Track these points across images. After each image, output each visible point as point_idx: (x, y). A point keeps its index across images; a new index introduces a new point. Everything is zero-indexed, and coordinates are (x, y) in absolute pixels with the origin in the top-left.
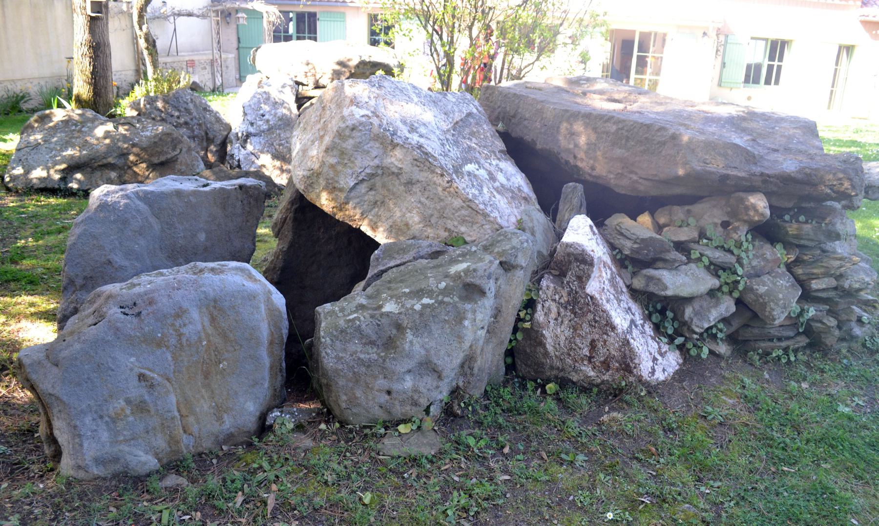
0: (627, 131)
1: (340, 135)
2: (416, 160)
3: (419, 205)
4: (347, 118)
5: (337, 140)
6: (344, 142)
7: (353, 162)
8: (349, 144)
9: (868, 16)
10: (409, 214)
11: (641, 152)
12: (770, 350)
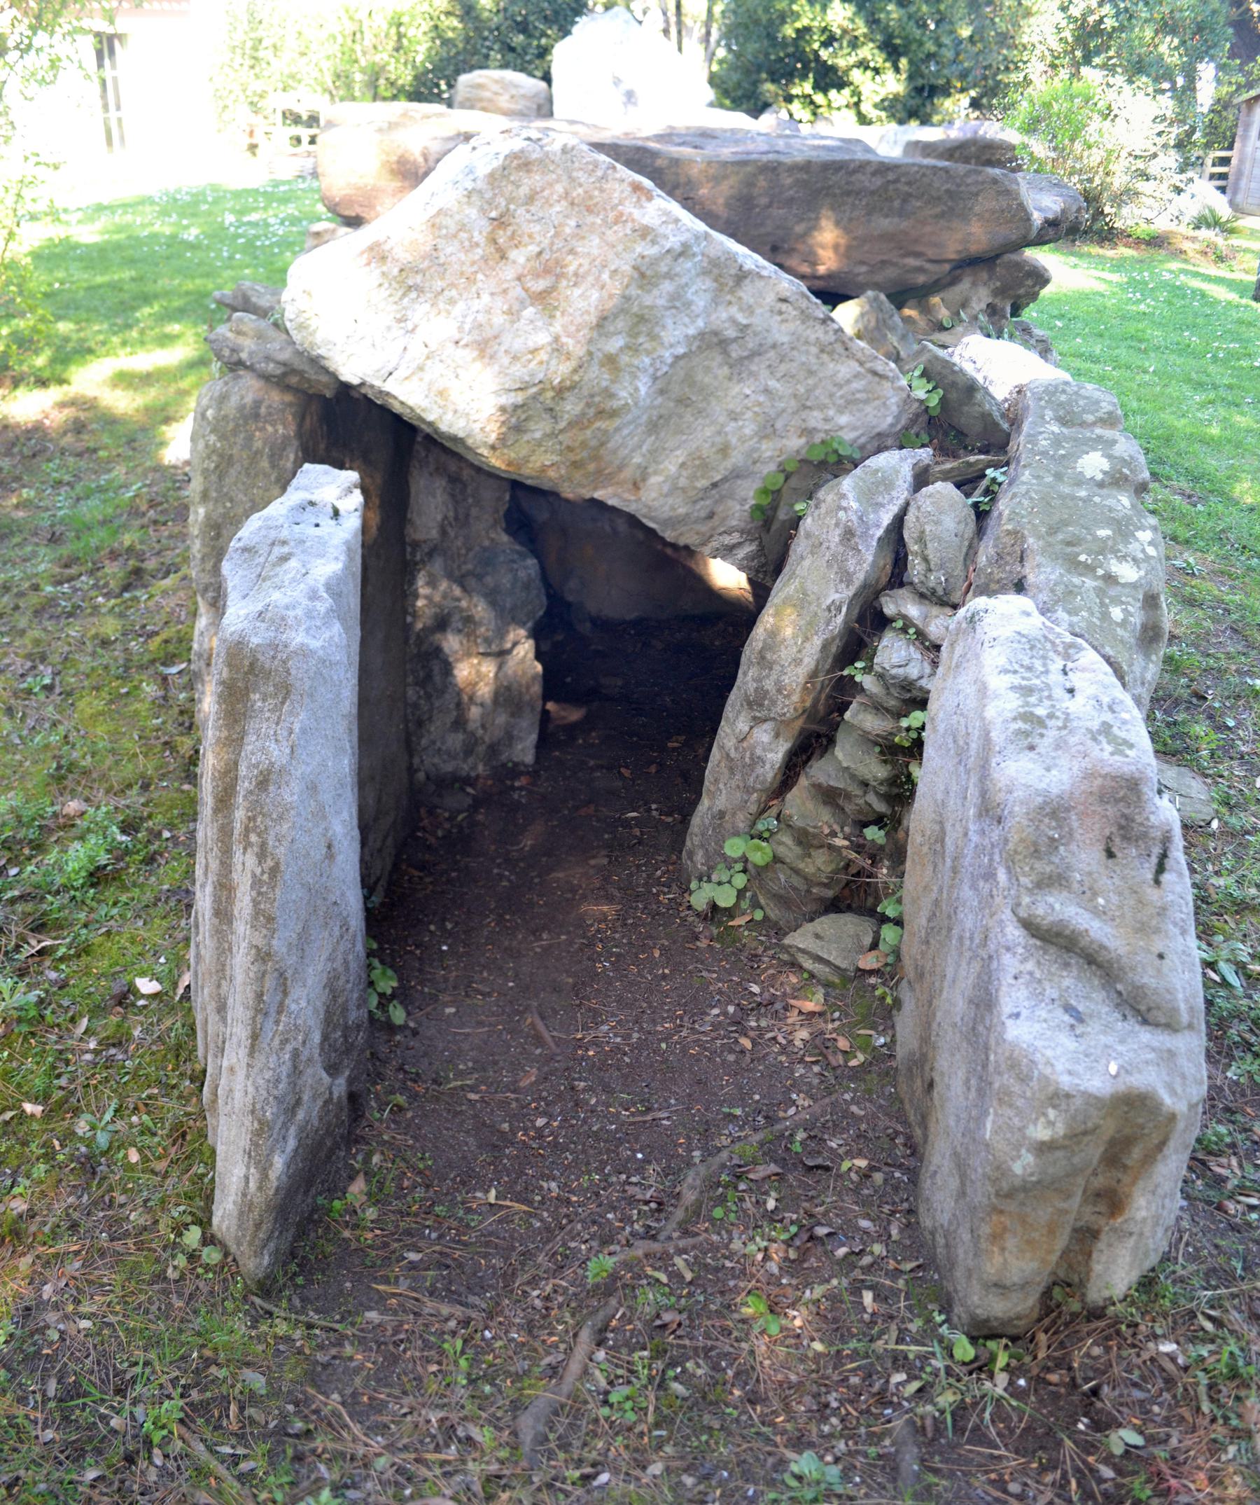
0: (909, 183)
1: (643, 275)
2: (784, 300)
3: (762, 399)
4: (662, 230)
5: (634, 291)
6: (649, 291)
7: (653, 337)
8: (658, 297)
9: (118, 108)
10: (733, 424)
11: (936, 216)
12: (718, 439)
